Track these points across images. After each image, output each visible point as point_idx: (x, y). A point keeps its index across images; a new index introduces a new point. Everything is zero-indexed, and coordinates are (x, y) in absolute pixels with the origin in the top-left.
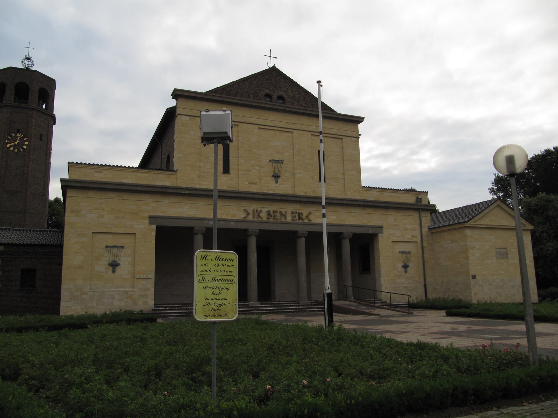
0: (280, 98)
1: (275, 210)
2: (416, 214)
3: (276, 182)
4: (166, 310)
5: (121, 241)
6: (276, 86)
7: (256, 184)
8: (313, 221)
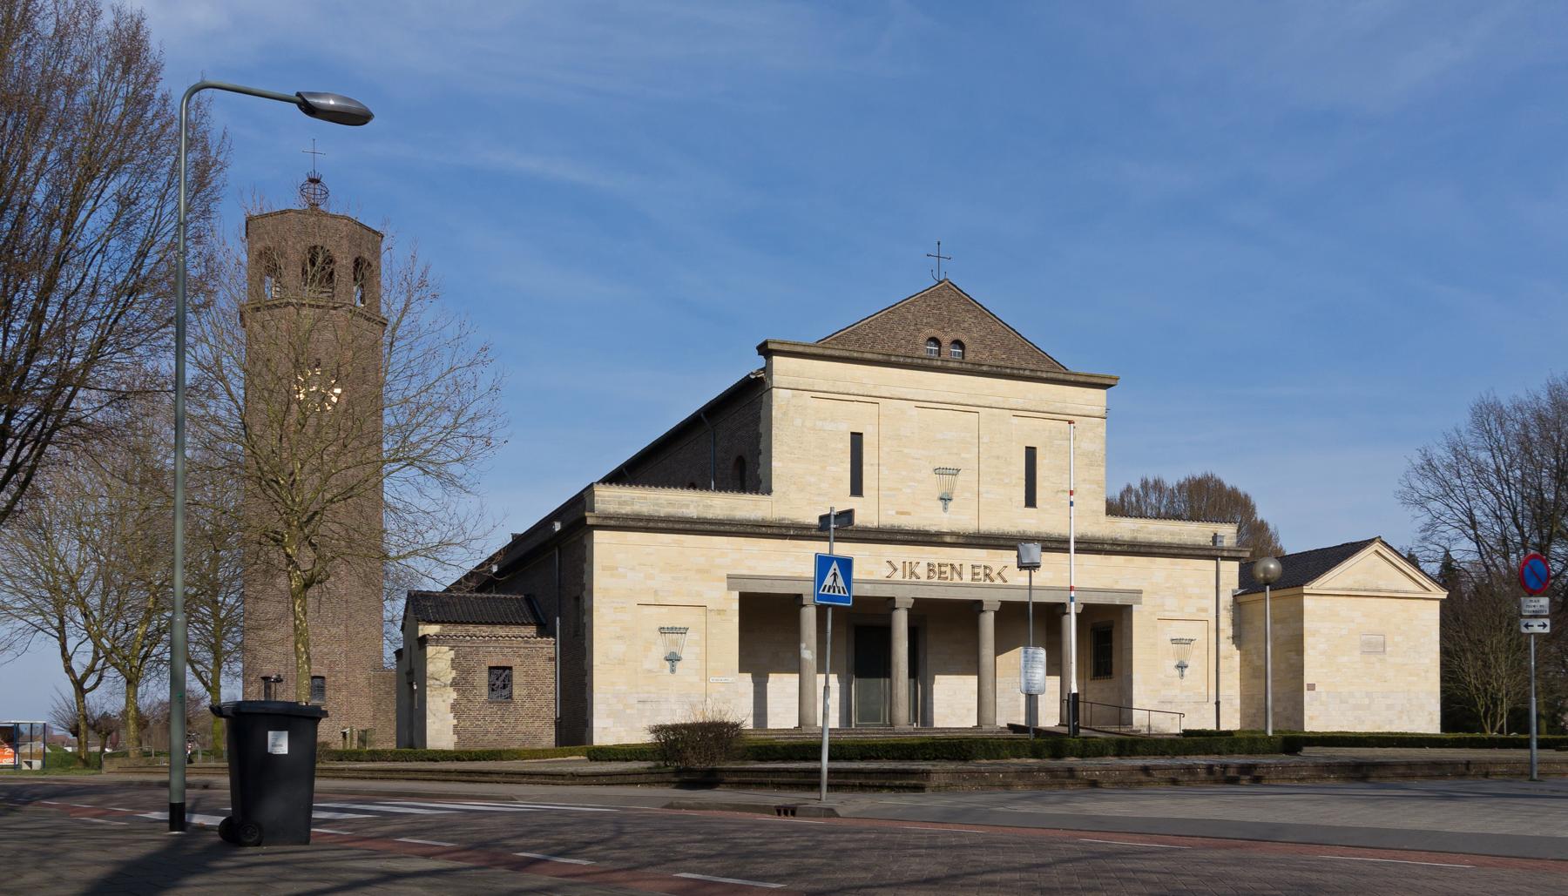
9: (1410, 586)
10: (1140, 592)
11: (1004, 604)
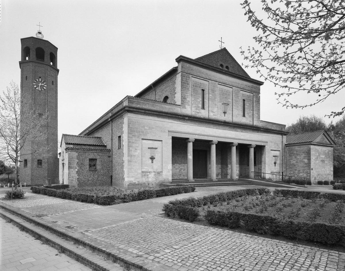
2: (280, 136)
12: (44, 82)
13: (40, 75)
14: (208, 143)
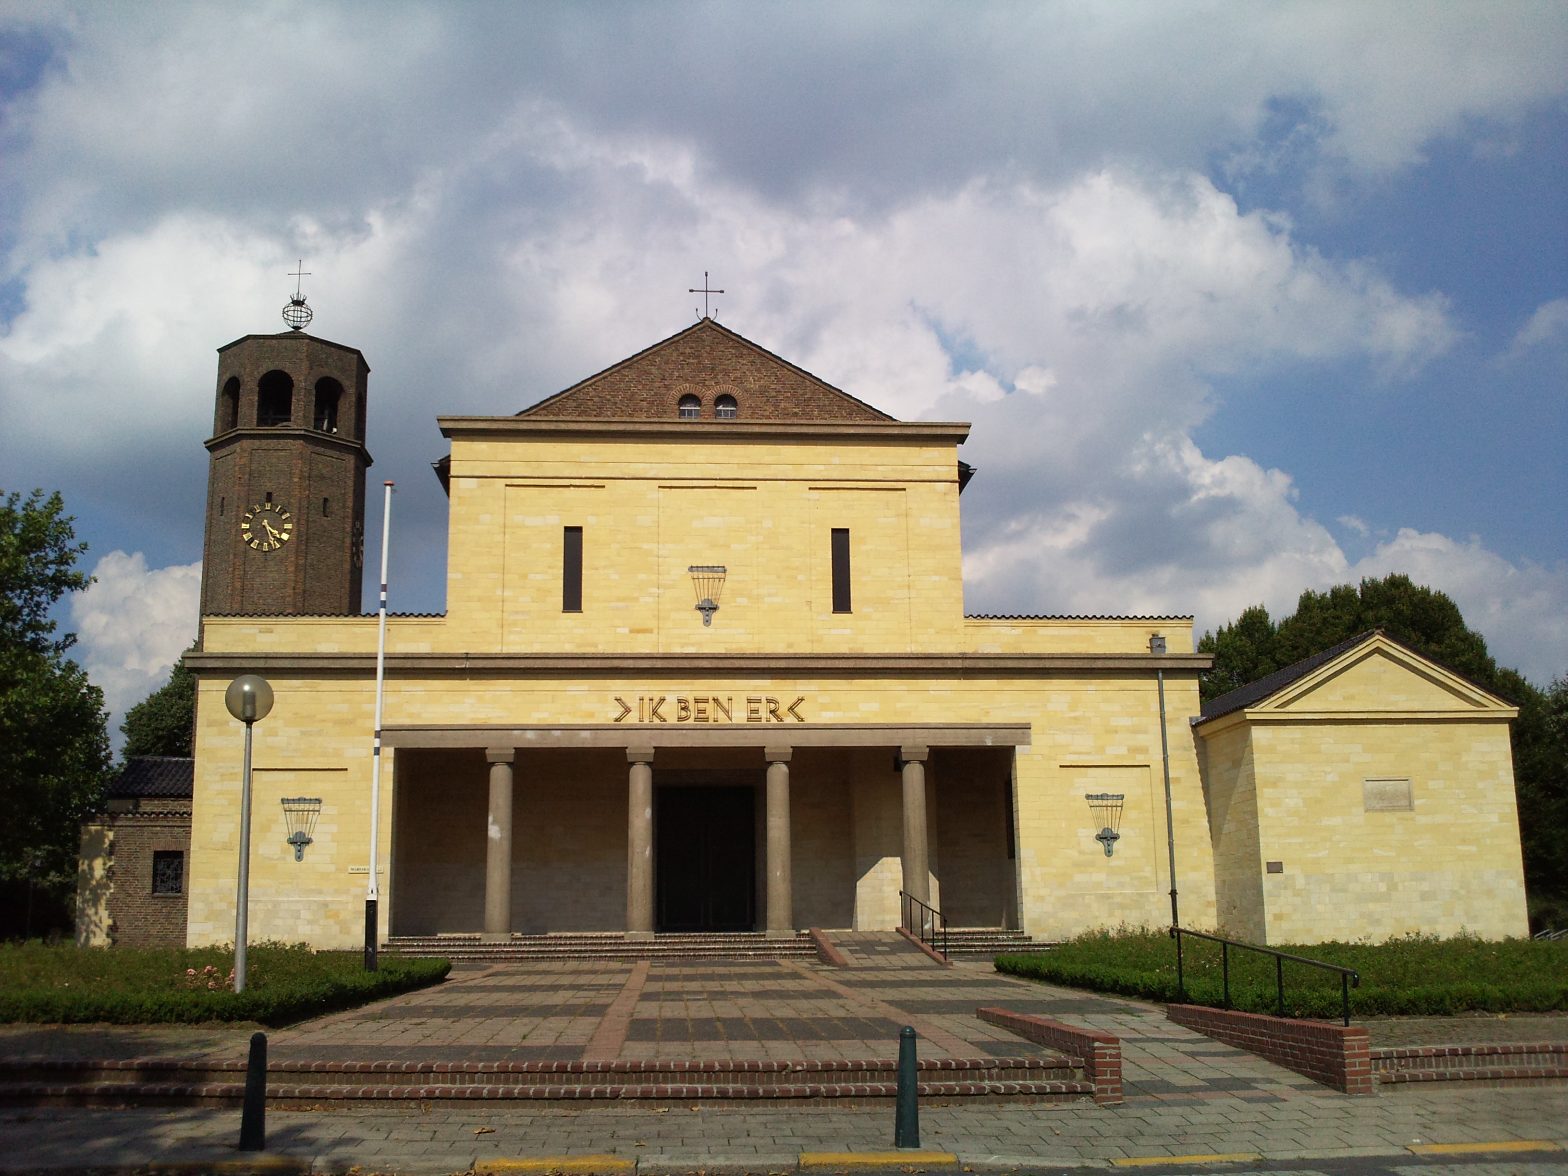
0: (725, 399)
1: (701, 695)
3: (707, 622)
4: (413, 946)
5: (312, 786)
6: (713, 369)
7: (649, 631)
8: (810, 720)
9: (1451, 704)
10: (1027, 727)
11: (798, 751)
12: (282, 514)
13: (268, 484)
14: (884, 762)
